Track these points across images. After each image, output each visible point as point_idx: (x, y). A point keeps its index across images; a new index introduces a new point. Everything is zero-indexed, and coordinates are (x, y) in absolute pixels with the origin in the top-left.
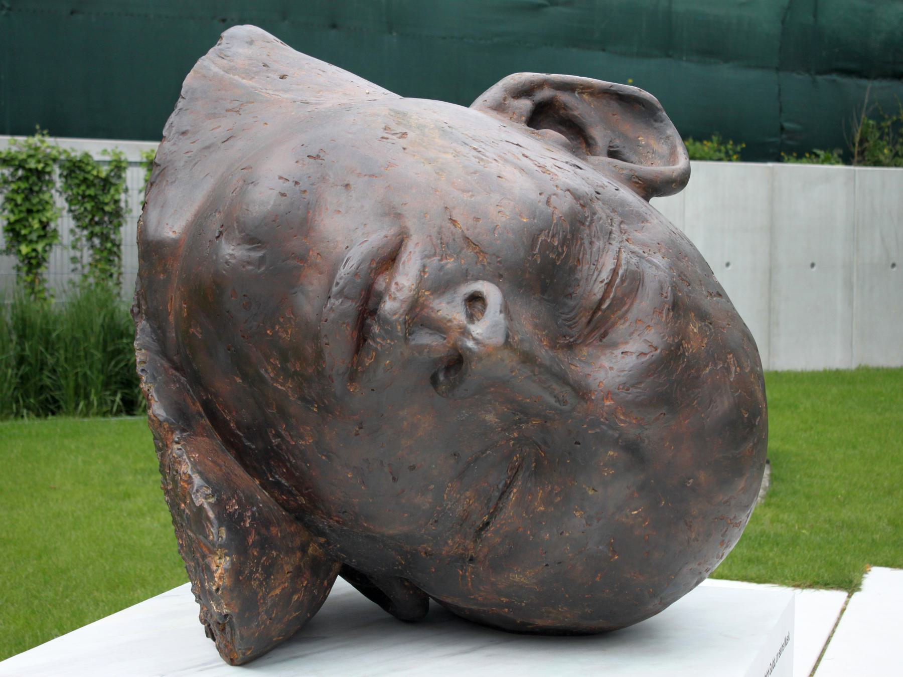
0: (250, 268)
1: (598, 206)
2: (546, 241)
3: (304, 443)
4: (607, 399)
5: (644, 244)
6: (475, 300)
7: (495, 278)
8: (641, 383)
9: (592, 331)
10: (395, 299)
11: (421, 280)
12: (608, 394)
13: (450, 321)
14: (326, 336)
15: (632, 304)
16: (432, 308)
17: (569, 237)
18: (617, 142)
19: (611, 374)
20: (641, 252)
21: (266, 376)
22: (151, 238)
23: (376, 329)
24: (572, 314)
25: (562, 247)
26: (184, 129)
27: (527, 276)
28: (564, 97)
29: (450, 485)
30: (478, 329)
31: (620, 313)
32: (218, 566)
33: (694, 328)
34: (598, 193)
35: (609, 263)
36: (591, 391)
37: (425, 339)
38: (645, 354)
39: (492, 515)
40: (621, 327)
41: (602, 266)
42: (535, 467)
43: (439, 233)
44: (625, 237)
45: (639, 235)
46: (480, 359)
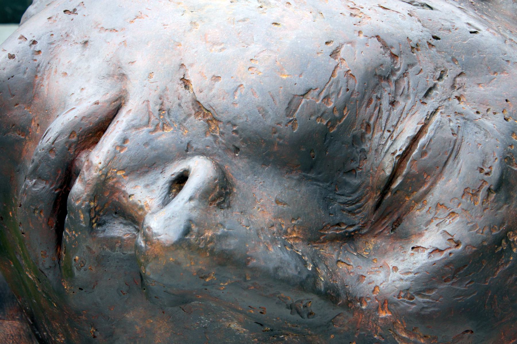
8: (430, 290)
9: (382, 217)
12: (385, 303)
15: (434, 184)
16: (124, 192)
19: (394, 276)
20: (472, 112)
24: (355, 196)
31: (416, 194)
35: (409, 128)
40: (418, 212)
44: (456, 93)
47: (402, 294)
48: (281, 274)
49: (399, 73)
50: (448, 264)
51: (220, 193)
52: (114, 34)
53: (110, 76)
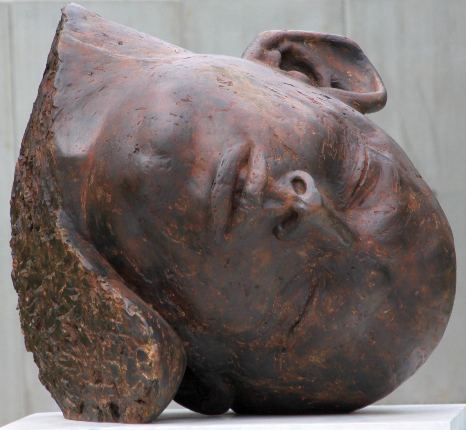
0: (162, 169)
1: (346, 121)
2: (326, 145)
3: (190, 275)
4: (369, 239)
5: (376, 145)
6: (298, 182)
7: (304, 168)
9: (355, 200)
10: (254, 183)
11: (267, 170)
12: (370, 237)
13: (286, 194)
14: (215, 206)
15: (377, 183)
16: (275, 187)
17: (337, 142)
18: (336, 76)
19: (369, 224)
21: (166, 235)
22: (65, 156)
23: (244, 201)
24: (342, 190)
25: (335, 149)
26: (69, 83)
27: (319, 167)
28: (298, 46)
29: (276, 298)
30: (305, 197)
31: (370, 188)
32: (149, 350)
33: (413, 196)
34: (344, 114)
35: (361, 159)
36: (359, 235)
37: (272, 205)
38: (388, 212)
39: (301, 316)
41: (359, 158)
42: (326, 285)
43: (270, 143)
45: (373, 140)
46: (309, 214)
47: (376, 232)
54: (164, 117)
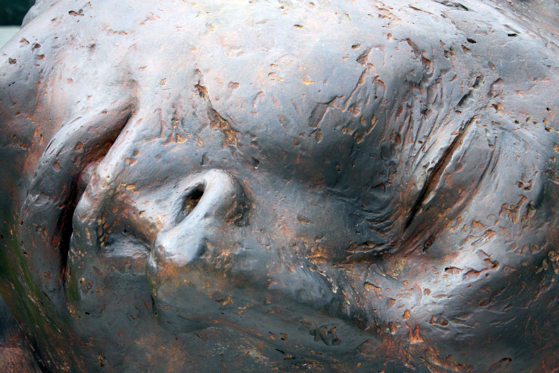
8: (465, 314)
9: (413, 235)
12: (416, 328)
15: (469, 199)
16: (134, 208)
19: (426, 299)
20: (511, 122)
24: (383, 213)
31: (450, 211)
35: (442, 139)
40: (452, 230)
44: (493, 101)
47: (435, 319)
48: (303, 297)
49: (431, 79)
50: (484, 286)
51: (238, 209)
52: (123, 37)
53: (119, 82)
54: (392, 68)
